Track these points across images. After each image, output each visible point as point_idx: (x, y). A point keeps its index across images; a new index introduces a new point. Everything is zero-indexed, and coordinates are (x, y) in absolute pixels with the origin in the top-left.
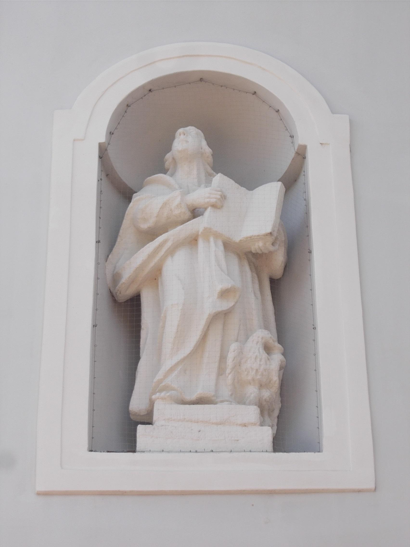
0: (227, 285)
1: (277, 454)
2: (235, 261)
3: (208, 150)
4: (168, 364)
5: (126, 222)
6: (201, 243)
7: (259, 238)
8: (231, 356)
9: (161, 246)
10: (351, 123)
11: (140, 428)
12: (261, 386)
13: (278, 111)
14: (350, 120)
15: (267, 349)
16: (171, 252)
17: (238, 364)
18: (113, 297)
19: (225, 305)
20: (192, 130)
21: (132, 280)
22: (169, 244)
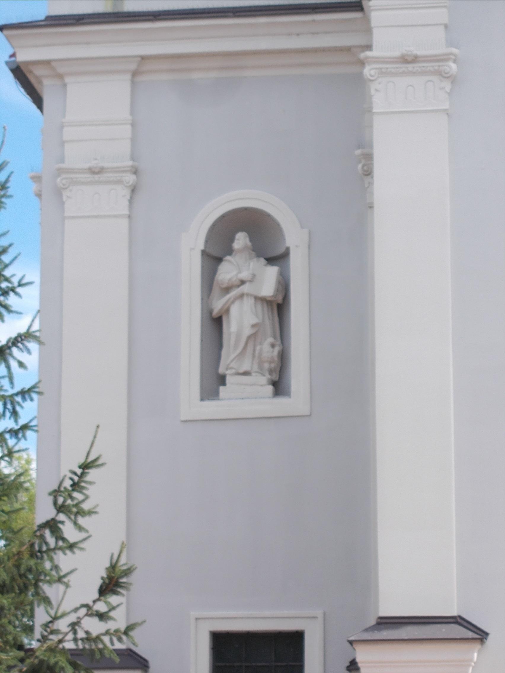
2: (259, 306)
15: (273, 346)
16: (233, 302)
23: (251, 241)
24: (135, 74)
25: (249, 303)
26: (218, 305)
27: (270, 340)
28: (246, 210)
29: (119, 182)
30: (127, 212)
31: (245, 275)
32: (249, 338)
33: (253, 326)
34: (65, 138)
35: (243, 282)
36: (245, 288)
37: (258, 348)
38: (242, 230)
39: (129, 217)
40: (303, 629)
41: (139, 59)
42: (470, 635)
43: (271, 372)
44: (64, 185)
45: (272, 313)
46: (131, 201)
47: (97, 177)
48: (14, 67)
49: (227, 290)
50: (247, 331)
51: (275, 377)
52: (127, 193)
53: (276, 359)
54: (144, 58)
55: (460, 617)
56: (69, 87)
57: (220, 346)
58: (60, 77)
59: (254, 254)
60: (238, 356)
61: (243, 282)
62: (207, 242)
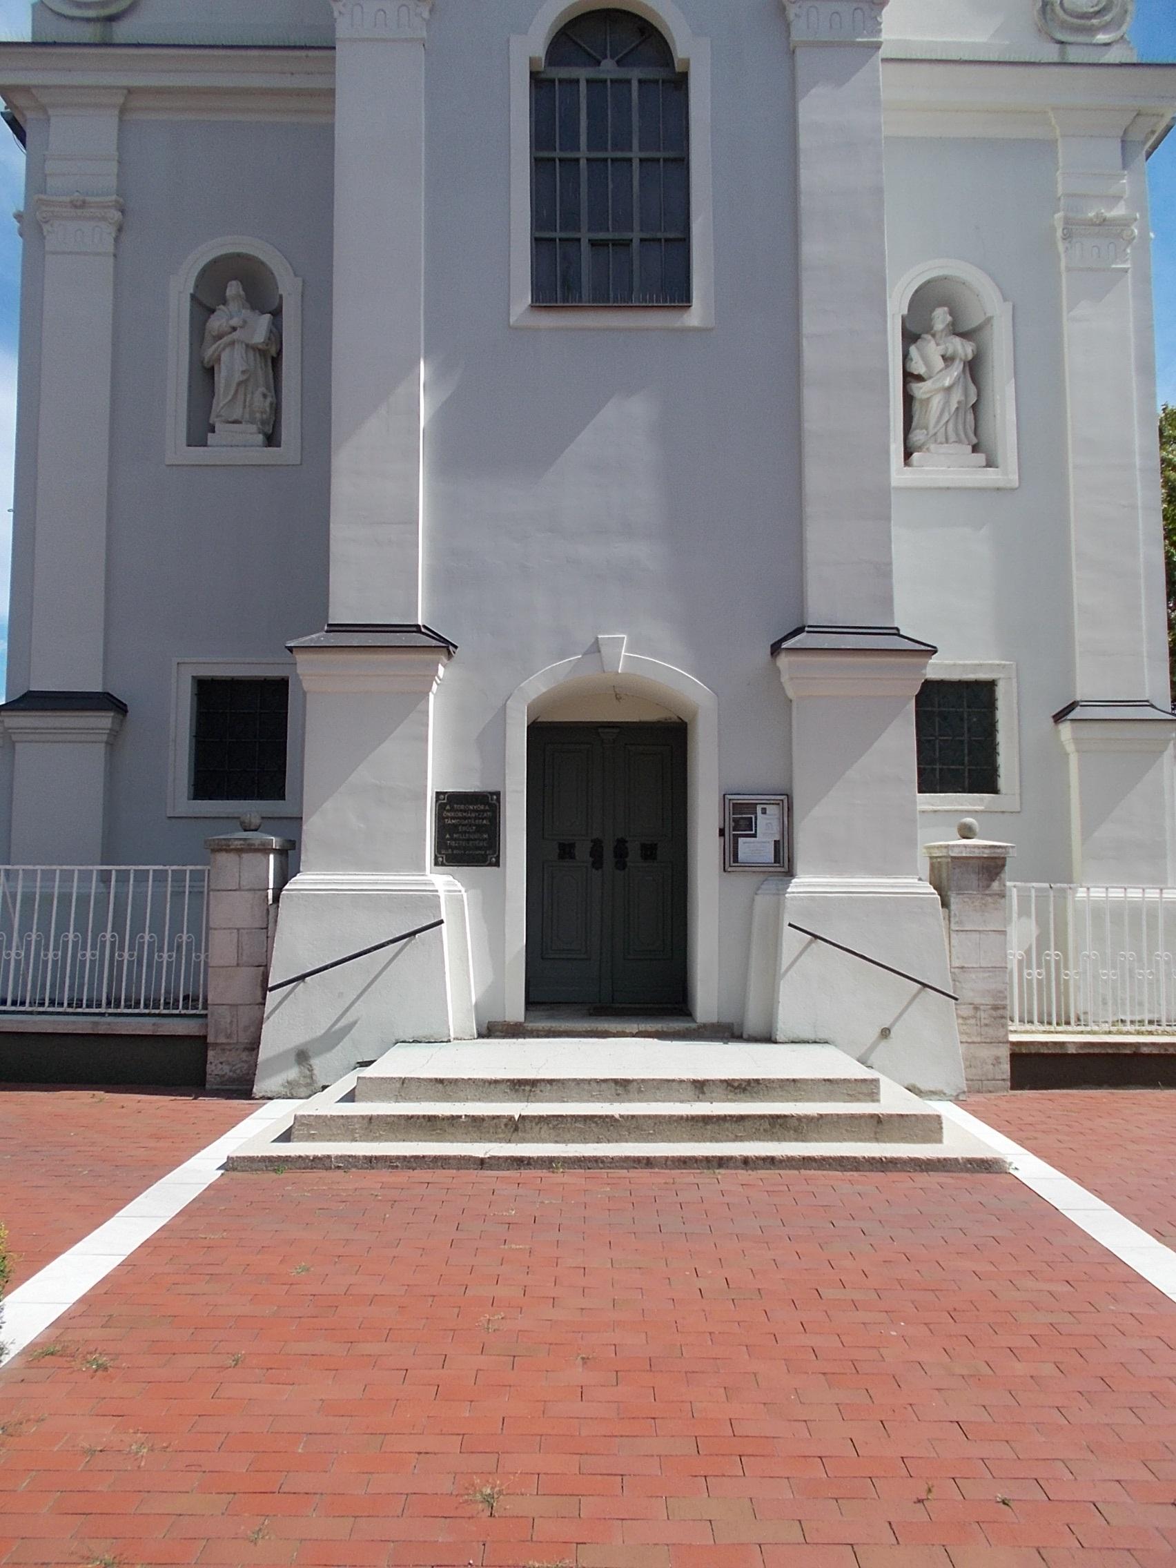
0: (244, 368)
1: (270, 449)
2: (251, 354)
3: (242, 293)
4: (221, 405)
5: (207, 334)
6: (236, 346)
7: (260, 344)
8: (248, 400)
9: (219, 347)
10: (1014, 307)
11: (16, 744)
12: (262, 413)
13: (964, 283)
14: (858, 1061)
15: (265, 396)
16: (224, 349)
17: (251, 404)
18: (204, 367)
19: (245, 377)
20: (234, 283)
21: (208, 362)
22: (222, 346)
23: (244, 290)
24: (123, 110)
25: (239, 351)
26: (209, 352)
27: (262, 389)
28: (239, 256)
29: (104, 219)
30: (111, 249)
31: (235, 322)
32: (239, 384)
33: (243, 372)
34: (47, 172)
35: (234, 329)
36: (235, 335)
37: (249, 396)
38: (235, 279)
39: (115, 256)
40: (283, 675)
41: (125, 91)
42: (434, 643)
43: (263, 423)
44: (44, 218)
45: (266, 366)
46: (117, 240)
47: (79, 212)
48: (9, 118)
49: (220, 337)
50: (238, 377)
51: (269, 429)
52: (112, 230)
53: (268, 409)
54: (130, 91)
55: (108, 694)
56: (53, 120)
57: (212, 392)
58: (43, 109)
59: (248, 305)
60: (227, 403)
61: (234, 329)
62: (196, 286)
